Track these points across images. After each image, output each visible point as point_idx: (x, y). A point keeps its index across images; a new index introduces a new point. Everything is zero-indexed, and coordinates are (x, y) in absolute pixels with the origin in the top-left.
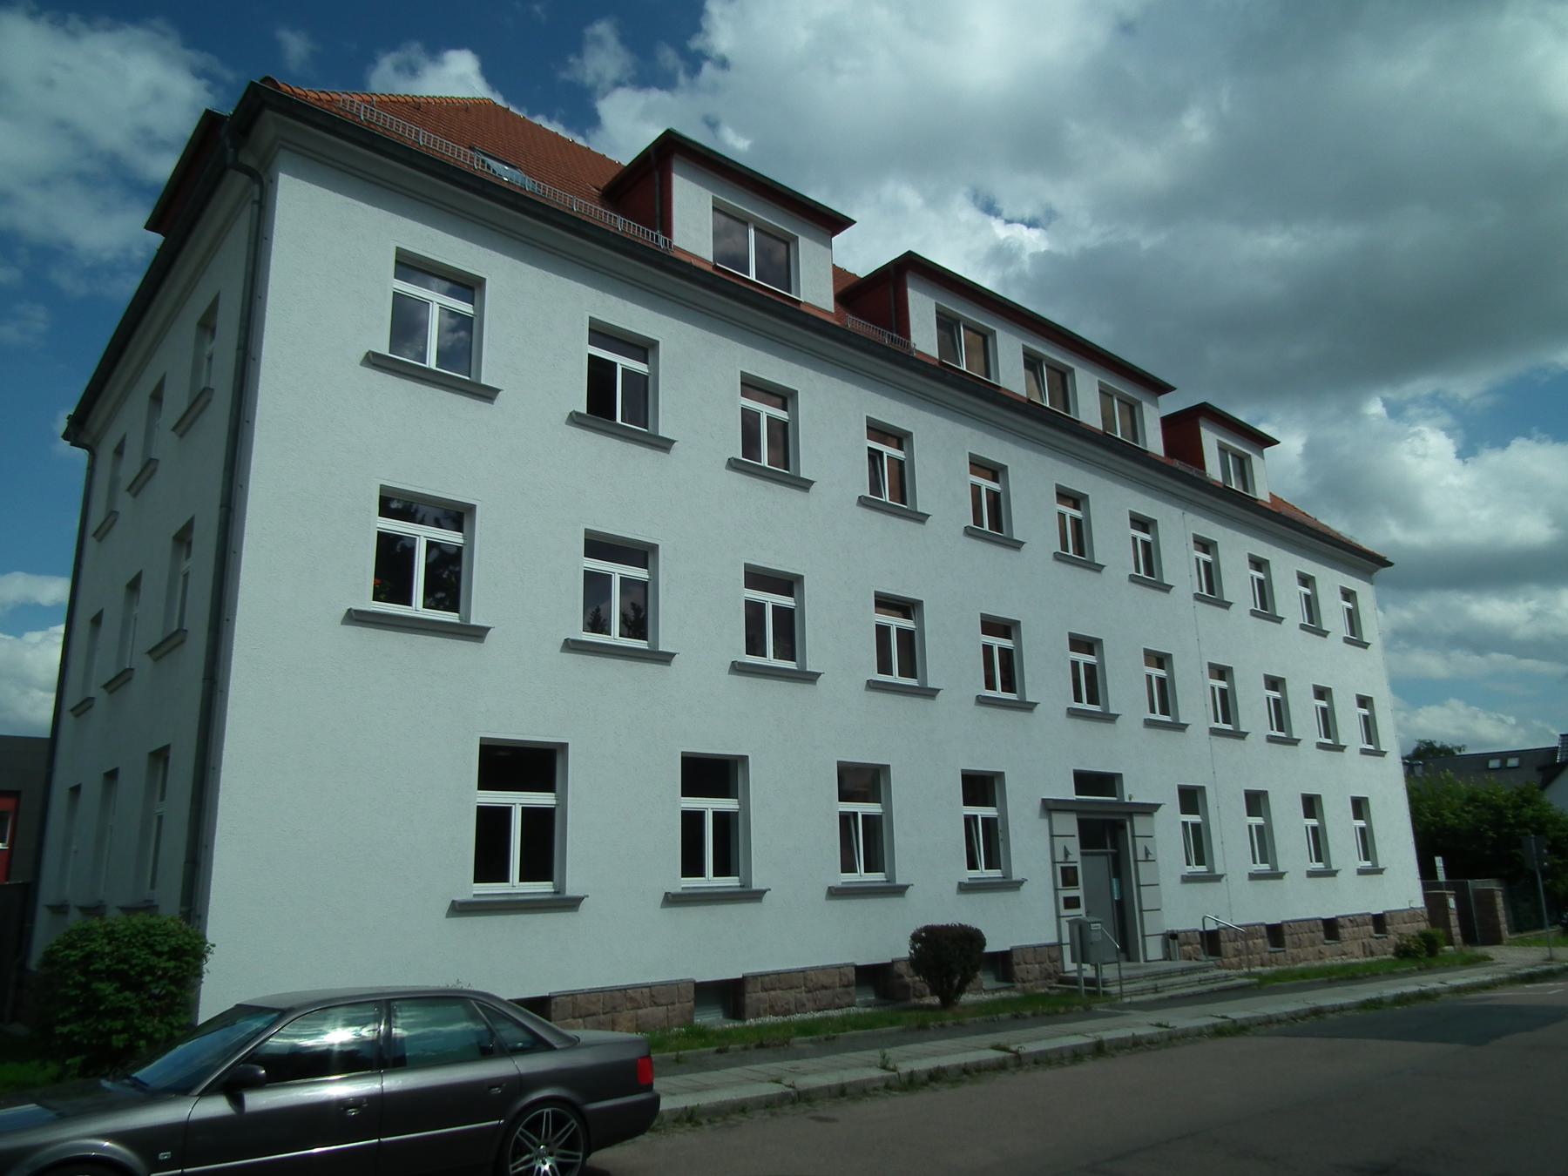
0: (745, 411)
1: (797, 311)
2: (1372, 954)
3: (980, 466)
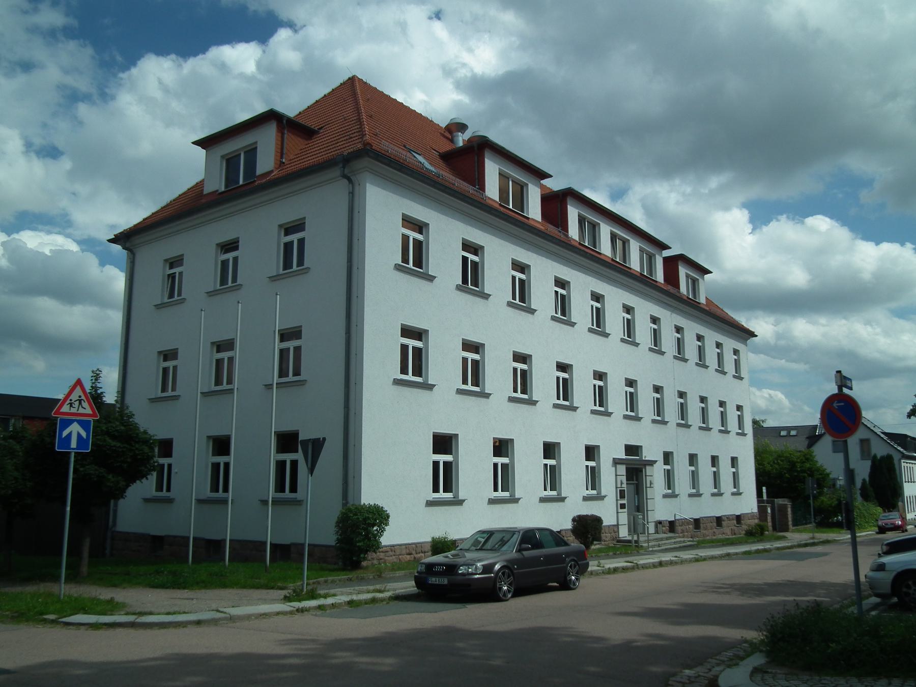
0: (555, 291)
1: (698, 306)
2: (735, 534)
3: (409, 222)
